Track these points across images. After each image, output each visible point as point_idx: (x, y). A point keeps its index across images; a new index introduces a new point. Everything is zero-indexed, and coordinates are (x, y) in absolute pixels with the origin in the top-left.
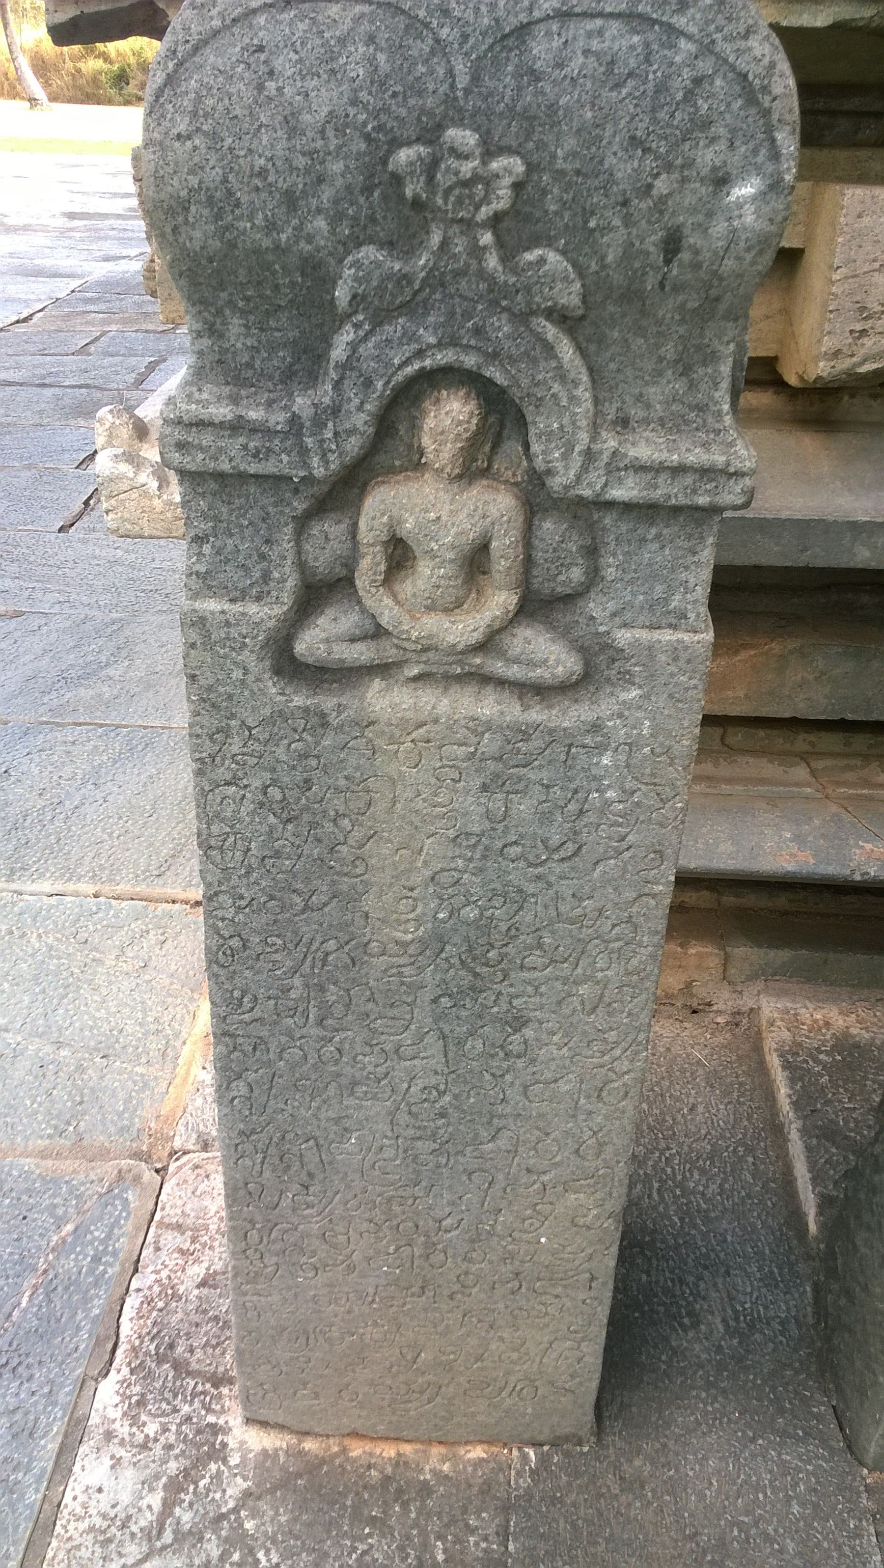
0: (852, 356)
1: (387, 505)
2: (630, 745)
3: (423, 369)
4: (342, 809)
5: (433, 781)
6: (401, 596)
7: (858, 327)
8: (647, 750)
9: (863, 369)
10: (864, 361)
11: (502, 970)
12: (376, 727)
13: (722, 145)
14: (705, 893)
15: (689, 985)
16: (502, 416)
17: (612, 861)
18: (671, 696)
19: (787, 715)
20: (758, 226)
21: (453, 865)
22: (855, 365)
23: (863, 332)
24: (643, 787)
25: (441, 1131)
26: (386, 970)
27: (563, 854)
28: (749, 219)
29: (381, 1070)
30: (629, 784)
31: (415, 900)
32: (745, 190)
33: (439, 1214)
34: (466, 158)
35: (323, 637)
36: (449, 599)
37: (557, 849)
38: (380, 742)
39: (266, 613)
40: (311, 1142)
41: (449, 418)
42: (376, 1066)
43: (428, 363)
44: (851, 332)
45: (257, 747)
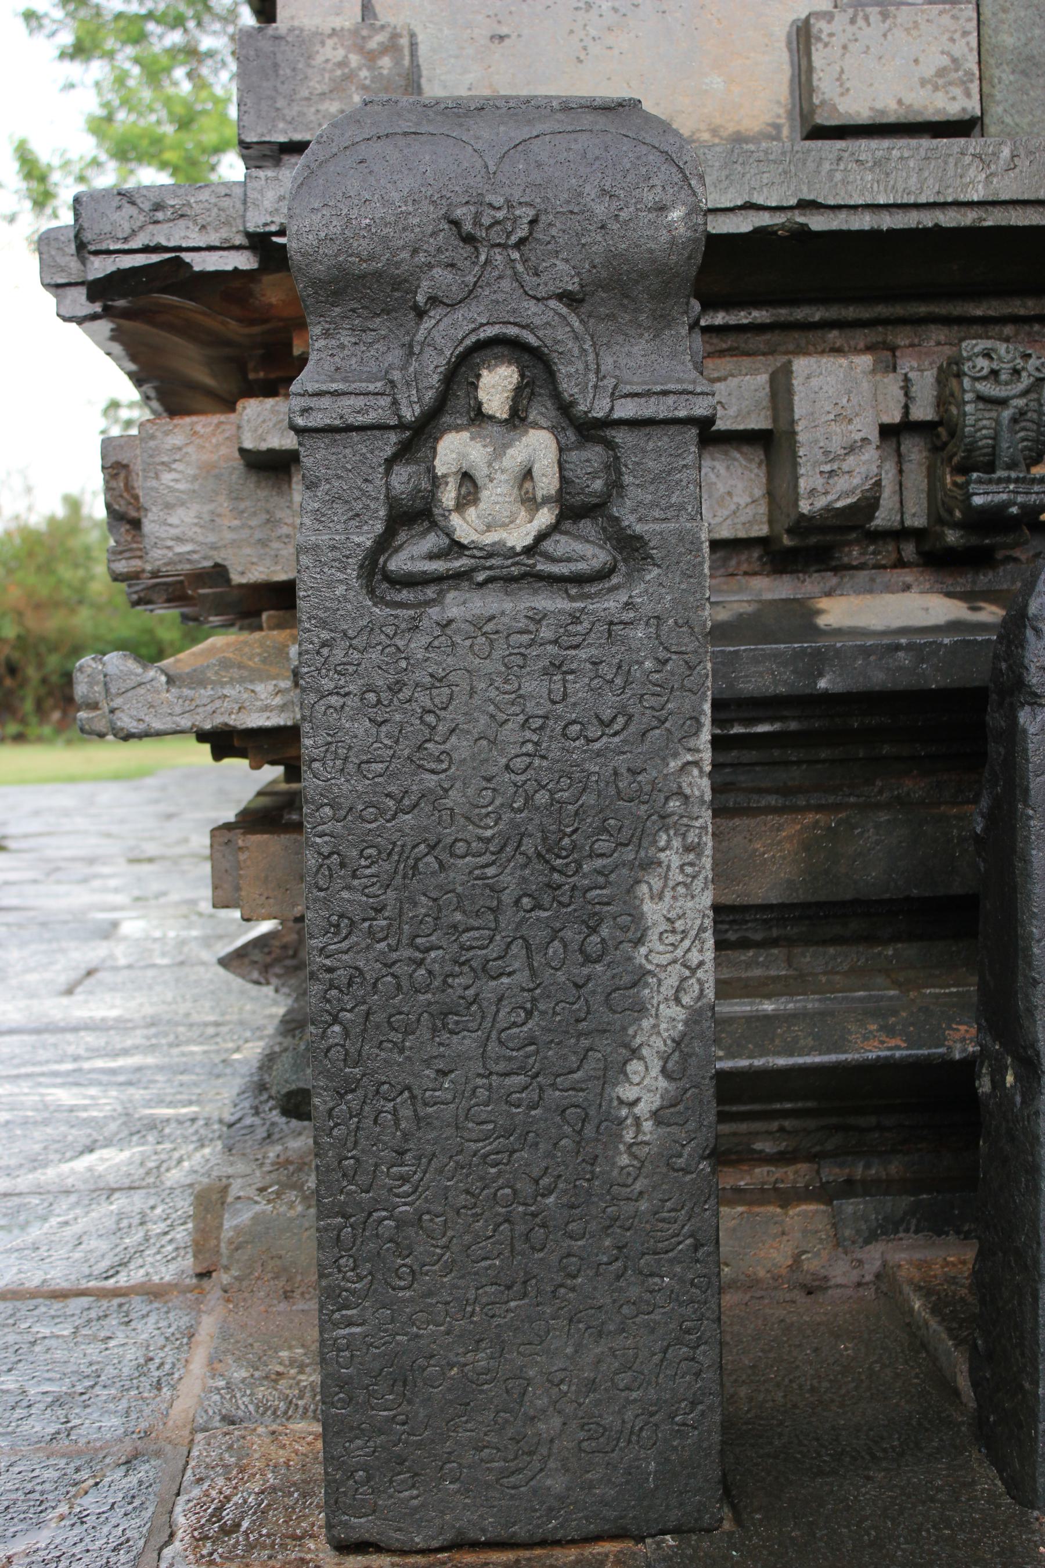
0: (826, 493)
1: (455, 449)
2: (657, 617)
3: (478, 340)
4: (429, 704)
5: (503, 669)
6: (469, 519)
7: (827, 468)
8: (671, 621)
9: (839, 505)
10: (838, 499)
11: (575, 861)
12: (454, 626)
13: (659, 189)
14: (803, 1167)
15: (797, 1259)
16: (535, 363)
17: (657, 731)
18: (683, 573)
19: (848, 897)
20: (689, 234)
21: (524, 750)
22: (832, 502)
23: (832, 473)
24: (674, 657)
25: (531, 1061)
26: (470, 872)
27: (617, 727)
28: (682, 230)
29: (471, 992)
30: (662, 654)
31: (494, 790)
32: (676, 214)
33: (536, 1172)
34: (499, 208)
35: (412, 556)
36: (505, 514)
37: (608, 725)
38: (458, 639)
39: (365, 539)
40: (406, 1094)
41: (496, 385)
42: (467, 988)
43: (482, 336)
44: (821, 472)
45: (356, 655)
